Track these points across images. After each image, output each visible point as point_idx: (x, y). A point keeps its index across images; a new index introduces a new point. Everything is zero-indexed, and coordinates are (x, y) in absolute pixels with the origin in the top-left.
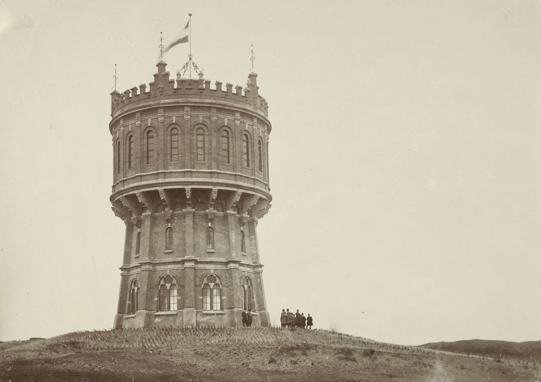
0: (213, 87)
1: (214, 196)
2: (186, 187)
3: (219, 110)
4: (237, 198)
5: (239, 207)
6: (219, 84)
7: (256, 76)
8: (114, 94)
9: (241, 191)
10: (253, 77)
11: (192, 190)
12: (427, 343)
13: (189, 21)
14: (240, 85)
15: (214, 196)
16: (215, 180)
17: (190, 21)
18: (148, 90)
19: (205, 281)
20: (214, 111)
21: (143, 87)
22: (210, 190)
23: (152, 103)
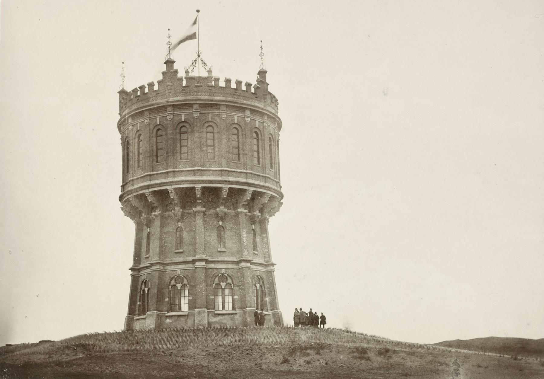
1: (225, 194)
4: (248, 196)
7: (265, 72)
8: (122, 93)
9: (252, 189)
10: (262, 73)
11: (230, 189)
16: (170, 180)
21: (151, 85)
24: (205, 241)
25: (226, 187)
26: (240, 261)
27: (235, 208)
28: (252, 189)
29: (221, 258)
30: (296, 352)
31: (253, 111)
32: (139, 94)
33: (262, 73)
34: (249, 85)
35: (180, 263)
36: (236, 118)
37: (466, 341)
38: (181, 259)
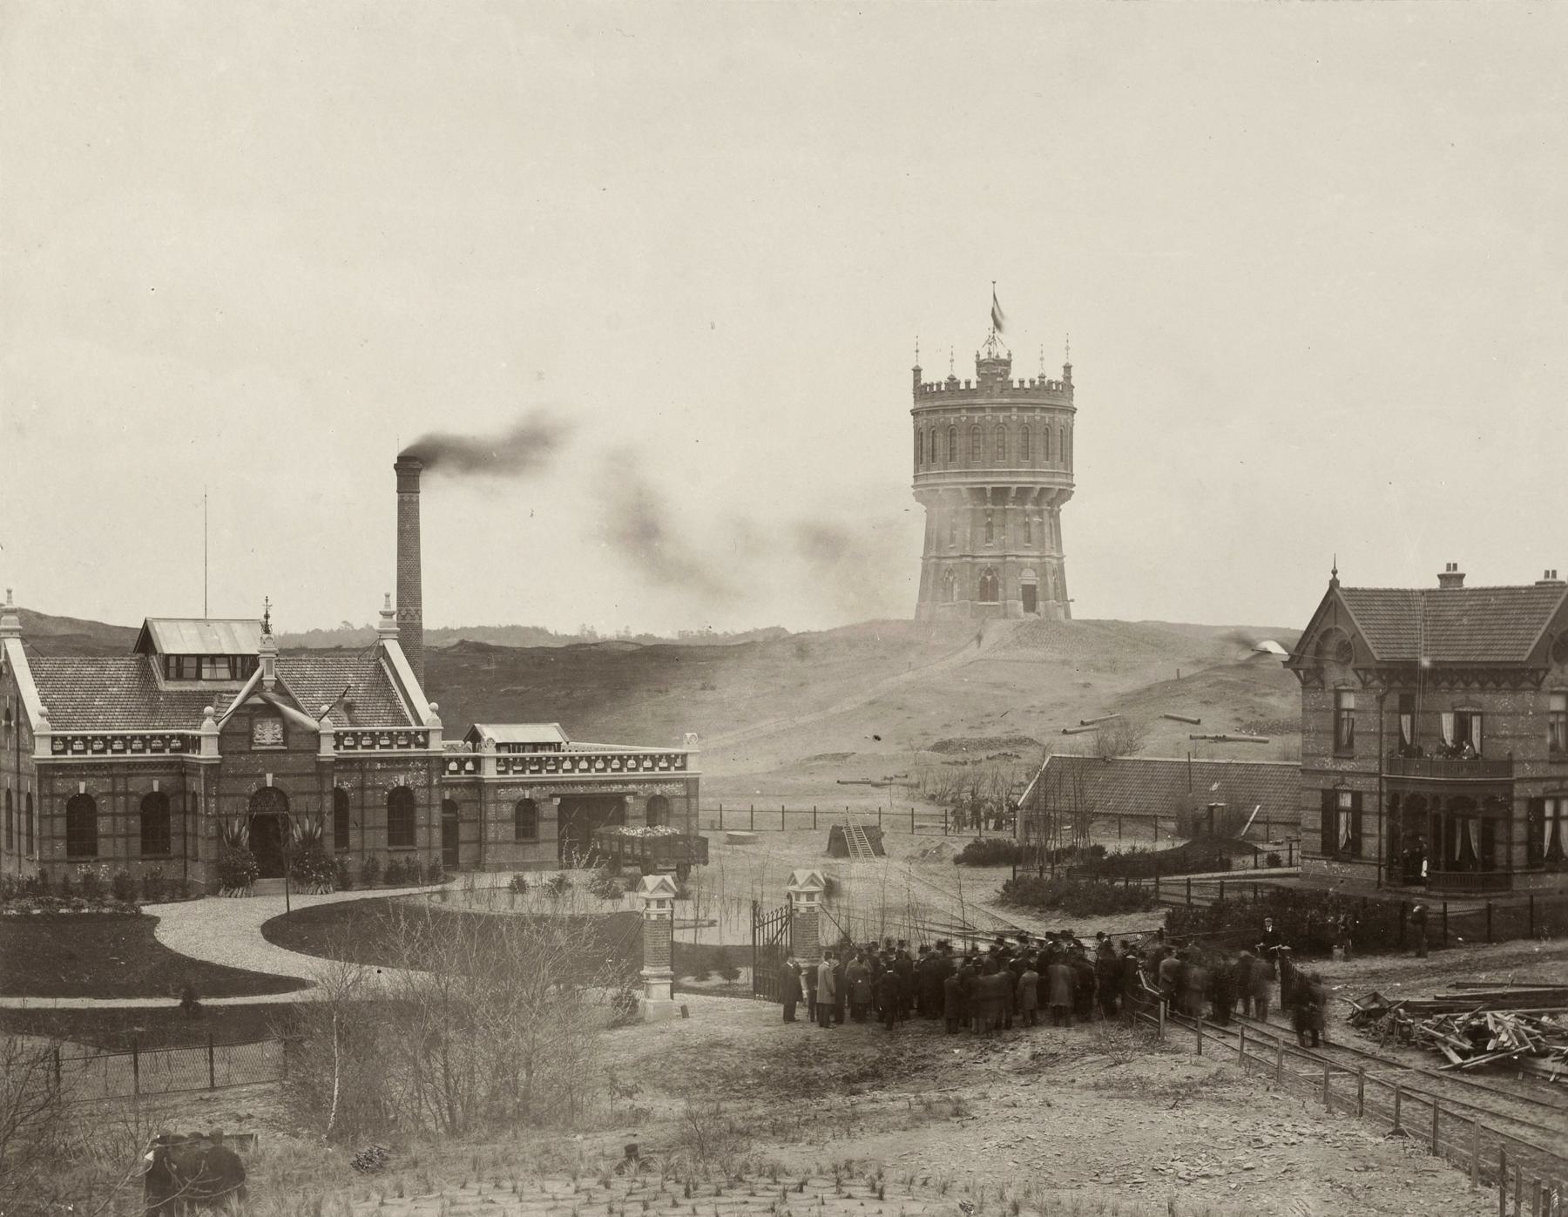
0: (963, 386)
1: (1013, 494)
2: (985, 486)
3: (945, 410)
4: (1035, 494)
5: (1037, 502)
6: (1022, 382)
7: (920, 371)
8: (921, 391)
9: (1016, 486)
10: (1067, 368)
11: (993, 488)
12: (1492, 585)
13: (993, 310)
14: (968, 378)
15: (1013, 494)
16: (1014, 479)
17: (996, 309)
18: (943, 388)
19: (983, 574)
20: (1038, 411)
21: (939, 385)
22: (1010, 488)
23: (980, 401)
24: (952, 534)
25: (1015, 487)
26: (1044, 557)
27: (1024, 504)
28: (1016, 486)
29: (1025, 553)
30: (1440, 679)
31: (1043, 409)
32: (935, 389)
33: (1067, 368)
34: (1032, 382)
35: (990, 557)
36: (976, 419)
37: (1127, 623)
38: (991, 553)
